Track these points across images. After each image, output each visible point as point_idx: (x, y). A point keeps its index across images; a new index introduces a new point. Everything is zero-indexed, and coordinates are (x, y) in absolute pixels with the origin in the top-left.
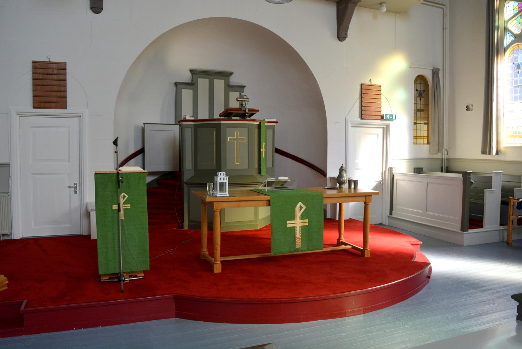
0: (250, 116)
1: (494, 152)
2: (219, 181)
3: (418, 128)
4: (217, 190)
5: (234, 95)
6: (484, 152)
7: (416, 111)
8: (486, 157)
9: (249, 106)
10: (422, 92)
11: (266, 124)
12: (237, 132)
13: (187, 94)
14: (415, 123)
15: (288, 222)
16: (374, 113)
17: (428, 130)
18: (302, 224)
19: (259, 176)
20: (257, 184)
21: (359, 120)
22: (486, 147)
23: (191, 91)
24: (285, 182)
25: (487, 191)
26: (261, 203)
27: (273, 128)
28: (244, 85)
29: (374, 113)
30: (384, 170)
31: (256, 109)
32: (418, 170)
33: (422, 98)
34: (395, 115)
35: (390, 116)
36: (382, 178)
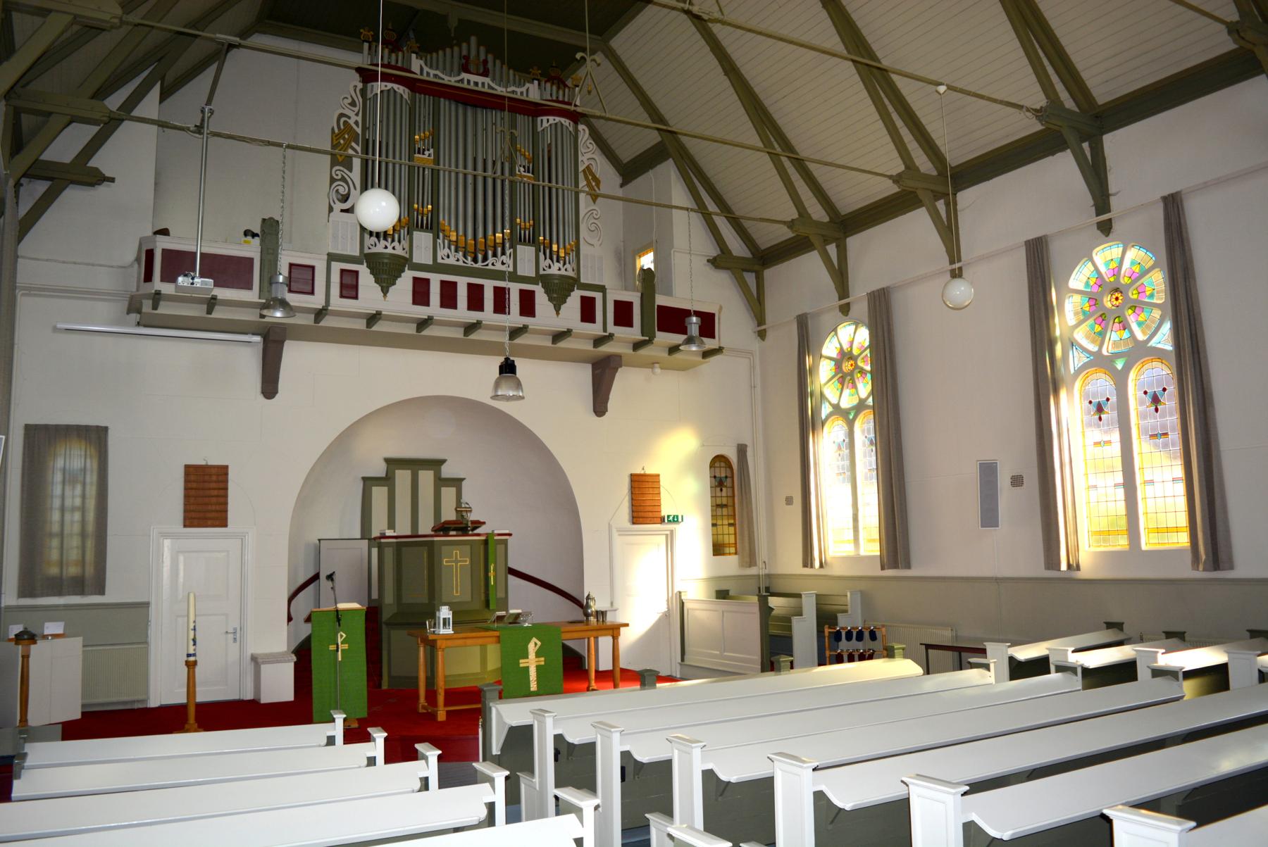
0: (472, 530)
1: (817, 564)
2: (442, 617)
3: (720, 532)
4: (439, 628)
5: (448, 494)
6: (805, 565)
7: (715, 508)
8: (808, 571)
9: (473, 517)
10: (724, 480)
11: (496, 538)
12: (456, 552)
13: (379, 494)
14: (714, 525)
15: (521, 661)
16: (651, 515)
17: (735, 534)
18: (538, 664)
19: (486, 610)
20: (485, 621)
21: (628, 525)
22: (807, 561)
23: (385, 489)
24: (518, 615)
25: (795, 620)
26: (491, 639)
27: (505, 542)
28: (462, 477)
29: (651, 515)
30: (670, 595)
31: (482, 521)
32: (722, 595)
33: (723, 489)
34: (682, 516)
35: (674, 518)
36: (668, 608)
